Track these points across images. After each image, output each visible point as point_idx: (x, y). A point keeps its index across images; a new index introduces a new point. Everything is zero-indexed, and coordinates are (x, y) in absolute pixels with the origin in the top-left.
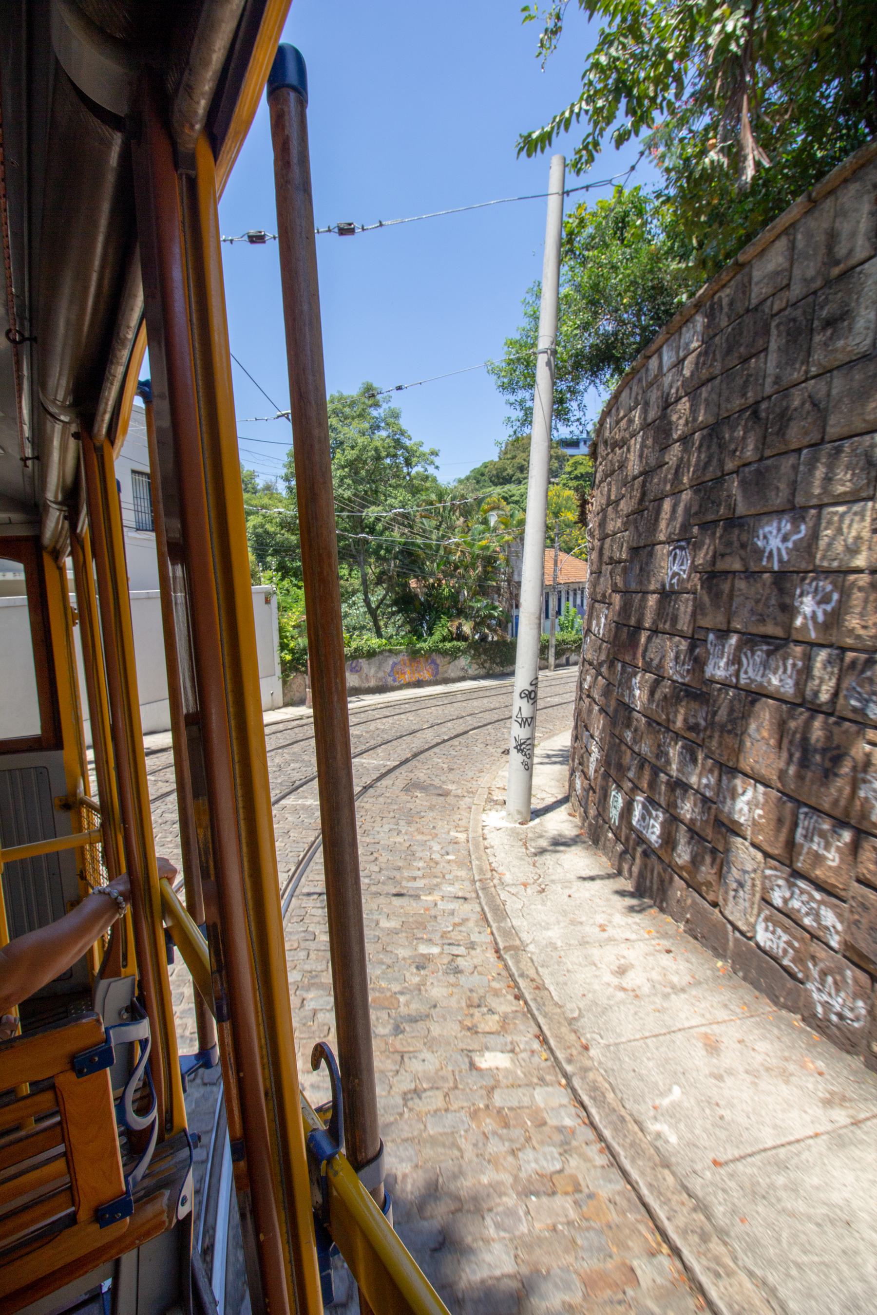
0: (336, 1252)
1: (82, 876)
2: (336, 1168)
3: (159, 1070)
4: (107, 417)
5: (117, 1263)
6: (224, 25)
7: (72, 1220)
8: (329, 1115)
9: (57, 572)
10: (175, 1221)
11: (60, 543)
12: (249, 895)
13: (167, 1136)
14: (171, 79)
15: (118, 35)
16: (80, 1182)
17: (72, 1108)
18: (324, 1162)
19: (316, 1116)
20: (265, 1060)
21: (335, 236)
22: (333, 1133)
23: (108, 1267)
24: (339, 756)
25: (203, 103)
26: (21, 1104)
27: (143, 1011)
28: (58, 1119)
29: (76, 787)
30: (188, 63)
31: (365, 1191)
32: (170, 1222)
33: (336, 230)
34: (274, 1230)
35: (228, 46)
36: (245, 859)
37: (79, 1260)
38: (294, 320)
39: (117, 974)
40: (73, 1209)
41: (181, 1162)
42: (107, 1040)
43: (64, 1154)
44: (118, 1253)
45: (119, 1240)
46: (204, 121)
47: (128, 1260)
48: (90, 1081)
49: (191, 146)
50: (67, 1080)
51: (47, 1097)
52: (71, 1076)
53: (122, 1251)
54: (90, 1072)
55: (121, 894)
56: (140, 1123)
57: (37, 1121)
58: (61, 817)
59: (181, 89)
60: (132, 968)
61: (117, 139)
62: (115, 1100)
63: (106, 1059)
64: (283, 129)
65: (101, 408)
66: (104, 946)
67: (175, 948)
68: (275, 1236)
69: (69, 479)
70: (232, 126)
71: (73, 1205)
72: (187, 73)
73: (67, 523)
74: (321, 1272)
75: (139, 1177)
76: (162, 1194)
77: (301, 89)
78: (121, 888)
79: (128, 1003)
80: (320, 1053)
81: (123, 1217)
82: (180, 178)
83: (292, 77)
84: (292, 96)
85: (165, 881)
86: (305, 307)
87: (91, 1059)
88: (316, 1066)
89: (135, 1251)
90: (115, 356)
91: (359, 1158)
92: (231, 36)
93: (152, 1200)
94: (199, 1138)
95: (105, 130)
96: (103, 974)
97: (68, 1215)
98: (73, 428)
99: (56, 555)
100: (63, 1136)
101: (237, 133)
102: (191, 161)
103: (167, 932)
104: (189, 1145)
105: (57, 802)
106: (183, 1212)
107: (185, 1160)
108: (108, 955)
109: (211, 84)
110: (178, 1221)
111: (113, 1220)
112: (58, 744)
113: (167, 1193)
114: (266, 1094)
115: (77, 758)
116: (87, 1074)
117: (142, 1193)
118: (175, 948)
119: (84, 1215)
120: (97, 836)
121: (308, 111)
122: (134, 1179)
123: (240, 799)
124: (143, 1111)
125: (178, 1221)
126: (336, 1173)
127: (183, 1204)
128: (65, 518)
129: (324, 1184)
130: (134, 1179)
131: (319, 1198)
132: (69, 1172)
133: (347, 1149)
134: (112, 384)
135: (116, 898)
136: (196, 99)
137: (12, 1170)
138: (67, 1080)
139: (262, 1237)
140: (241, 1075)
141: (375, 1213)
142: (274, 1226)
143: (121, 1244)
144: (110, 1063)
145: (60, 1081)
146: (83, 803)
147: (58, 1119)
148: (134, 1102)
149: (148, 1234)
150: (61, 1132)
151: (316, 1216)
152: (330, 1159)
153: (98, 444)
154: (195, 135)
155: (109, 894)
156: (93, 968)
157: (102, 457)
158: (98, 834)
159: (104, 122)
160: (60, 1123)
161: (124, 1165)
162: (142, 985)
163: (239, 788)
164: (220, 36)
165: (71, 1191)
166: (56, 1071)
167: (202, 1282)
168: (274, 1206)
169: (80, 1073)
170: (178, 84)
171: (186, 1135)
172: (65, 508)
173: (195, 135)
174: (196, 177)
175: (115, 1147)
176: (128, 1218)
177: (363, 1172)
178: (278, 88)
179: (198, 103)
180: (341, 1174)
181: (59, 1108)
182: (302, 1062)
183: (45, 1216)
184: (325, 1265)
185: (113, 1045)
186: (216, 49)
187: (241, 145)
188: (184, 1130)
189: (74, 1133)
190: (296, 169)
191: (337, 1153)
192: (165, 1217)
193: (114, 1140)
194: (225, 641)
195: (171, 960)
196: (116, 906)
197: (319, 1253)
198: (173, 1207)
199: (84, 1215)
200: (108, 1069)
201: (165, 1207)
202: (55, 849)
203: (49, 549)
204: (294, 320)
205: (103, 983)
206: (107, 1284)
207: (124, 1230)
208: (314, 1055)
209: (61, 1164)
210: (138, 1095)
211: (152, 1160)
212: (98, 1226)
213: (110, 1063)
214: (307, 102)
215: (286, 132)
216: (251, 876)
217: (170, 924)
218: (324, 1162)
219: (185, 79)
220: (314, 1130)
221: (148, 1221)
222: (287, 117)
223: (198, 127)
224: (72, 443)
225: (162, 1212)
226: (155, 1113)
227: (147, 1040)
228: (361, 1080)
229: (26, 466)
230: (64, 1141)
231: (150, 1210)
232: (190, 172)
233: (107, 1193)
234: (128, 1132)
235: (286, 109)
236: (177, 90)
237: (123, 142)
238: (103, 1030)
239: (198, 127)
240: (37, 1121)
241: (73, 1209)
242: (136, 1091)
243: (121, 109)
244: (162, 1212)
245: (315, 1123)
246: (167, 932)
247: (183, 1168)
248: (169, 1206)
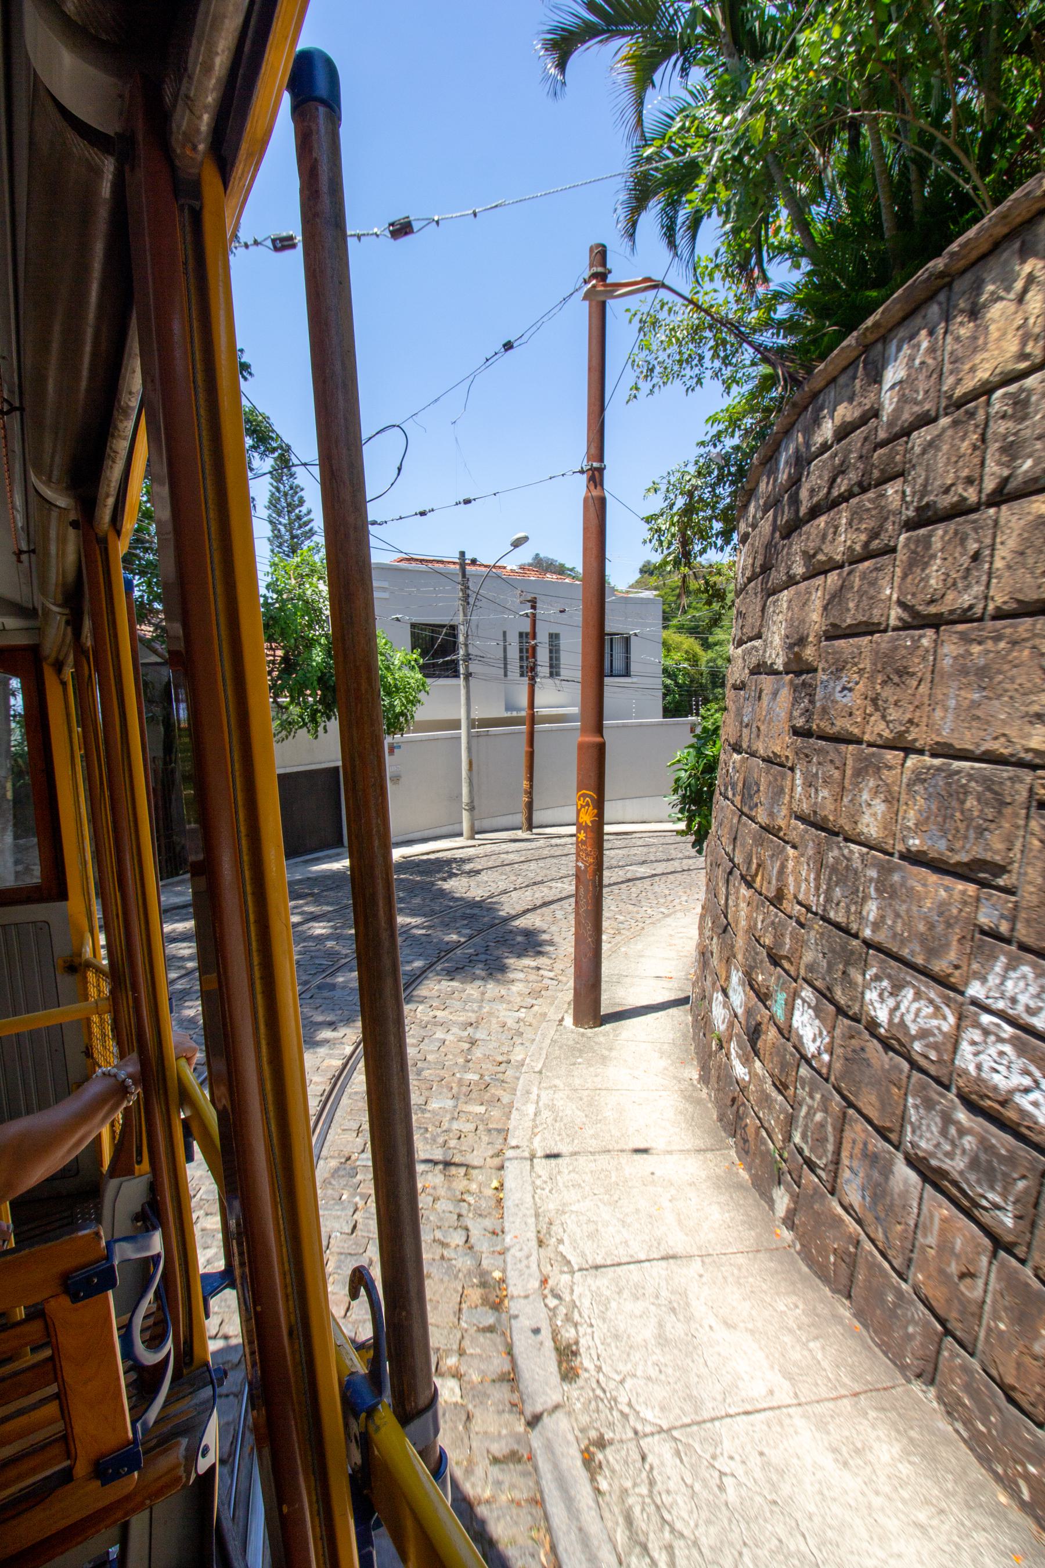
0: (378, 1524)
1: (88, 1053)
2: (378, 1422)
3: (176, 1291)
4: (111, 501)
5: (125, 1528)
6: (227, 21)
7: (66, 1476)
8: (371, 1353)
9: (60, 688)
10: (193, 1476)
11: (62, 654)
12: (268, 1086)
13: (185, 1371)
14: (168, 91)
15: (104, 37)
16: (77, 1430)
17: (67, 1340)
18: (363, 1415)
19: (354, 1356)
20: (289, 1290)
21: (265, 252)
22: (375, 1375)
23: (115, 1531)
24: (381, 913)
25: (206, 117)
26: (18, 1330)
27: (155, 1221)
28: (47, 1353)
29: (82, 944)
30: (186, 69)
31: (413, 1451)
32: (188, 1478)
33: (269, 243)
34: (301, 1501)
35: (233, 47)
36: (263, 1043)
37: (90, 1517)
38: (324, 382)
39: (130, 1172)
40: (68, 1463)
41: (202, 1403)
42: (109, 1257)
43: (57, 1396)
44: (126, 1514)
45: (127, 1498)
46: (210, 140)
47: (138, 1523)
48: (87, 1309)
49: (194, 171)
50: (60, 1307)
51: (37, 1326)
52: (65, 1301)
53: (134, 1511)
54: (88, 1296)
55: (130, 1076)
56: (150, 1358)
57: (33, 1350)
58: (66, 982)
59: (180, 102)
60: (146, 1166)
61: (109, 166)
62: (119, 1329)
63: (107, 1279)
64: (310, 151)
65: (103, 490)
66: (114, 1138)
67: (196, 1146)
68: (302, 1508)
69: (71, 576)
70: (244, 146)
71: (69, 1457)
72: (185, 80)
73: (69, 629)
74: (360, 1549)
75: (151, 1422)
76: (178, 1444)
77: (332, 104)
78: (130, 1069)
79: (139, 1209)
80: (359, 1280)
81: (131, 1471)
82: (181, 208)
83: (322, 88)
84: (322, 110)
85: (183, 1062)
86: (338, 367)
87: (89, 1279)
88: (354, 1295)
89: (147, 1513)
90: (116, 428)
91: (408, 1408)
92: (236, 34)
93: (166, 1451)
94: (225, 1373)
95: (92, 154)
96: (113, 1172)
97: (64, 1469)
98: (73, 516)
99: (59, 666)
100: (55, 1373)
101: (250, 155)
102: (195, 190)
103: (185, 1123)
104: (212, 1382)
105: (60, 962)
106: (203, 1465)
107: (208, 1401)
108: (119, 1149)
109: (214, 95)
110: (198, 1476)
111: (117, 1476)
112: (62, 895)
113: (184, 1442)
114: (291, 1333)
115: (83, 909)
116: (83, 1298)
117: (155, 1441)
118: (196, 1146)
119: (81, 1469)
120: (105, 1005)
121: (343, 131)
122: (144, 1424)
123: (256, 968)
124: (155, 1342)
125: (198, 1476)
126: (378, 1428)
127: (204, 1456)
128: (67, 623)
129: (365, 1442)
130: (144, 1424)
131: (357, 1458)
132: (63, 1417)
133: (394, 1396)
134: (114, 462)
135: (124, 1081)
136: (198, 113)
137: (11, 1408)
138: (60, 1307)
139: (285, 1509)
140: (259, 1308)
141: (424, 1479)
142: (300, 1494)
143: (128, 1504)
144: (113, 1285)
145: (52, 1306)
146: (88, 965)
147: (47, 1353)
148: (142, 1331)
149: (160, 1492)
150: (52, 1369)
151: (352, 1478)
152: (371, 1411)
153: (101, 534)
154: (199, 157)
155: (115, 1076)
156: (100, 1163)
157: (106, 549)
158: (106, 1002)
159: (92, 143)
160: (51, 1359)
161: (130, 1410)
162: (154, 1188)
163: (255, 954)
164: (223, 34)
165: (66, 1440)
166: (45, 1295)
167: (233, 1546)
168: (300, 1470)
169: (75, 1298)
170: (176, 96)
171: (209, 1370)
172: (67, 611)
173: (199, 157)
174: (201, 208)
175: (119, 1385)
176: (136, 1474)
177: (413, 1426)
178: (304, 101)
179: (200, 118)
180: (383, 1430)
181: (49, 1339)
182: (337, 1290)
183: (34, 1471)
184: (365, 1541)
185: (116, 1263)
186: (219, 51)
187: (257, 170)
188: (207, 1364)
189: (68, 1370)
190: (326, 200)
191: (378, 1404)
192: (181, 1472)
193: (118, 1378)
194: (237, 774)
195: (190, 1158)
196: (122, 1090)
197: (356, 1527)
198: (191, 1458)
199: (81, 1469)
200: (110, 1293)
201: (182, 1460)
202: (14, 1031)
203: (51, 660)
204: (324, 382)
205: (113, 1183)
206: (114, 1551)
207: (132, 1487)
208: (352, 1281)
209: (52, 1409)
210: (151, 1321)
211: (166, 1401)
212: (99, 1483)
213: (113, 1285)
214: (340, 119)
215: (314, 155)
216: (271, 1062)
217: (189, 1113)
218: (363, 1415)
219: (183, 89)
220: (352, 1373)
221: (160, 1477)
222: (314, 137)
223: (201, 147)
224: (71, 533)
225: (178, 1466)
226: (169, 1344)
227: (159, 1255)
228: (409, 1313)
229: (19, 561)
230: (56, 1380)
231: (164, 1463)
232: (196, 204)
233: (109, 1441)
234: (135, 1366)
235: (314, 127)
236: (174, 106)
237: (116, 168)
238: (103, 1243)
239: (201, 147)
240: (33, 1350)
241: (68, 1463)
242: (145, 1318)
243: (110, 127)
244: (178, 1466)
245: (353, 1365)
246: (185, 1123)
247: (204, 1411)
248: (186, 1458)
